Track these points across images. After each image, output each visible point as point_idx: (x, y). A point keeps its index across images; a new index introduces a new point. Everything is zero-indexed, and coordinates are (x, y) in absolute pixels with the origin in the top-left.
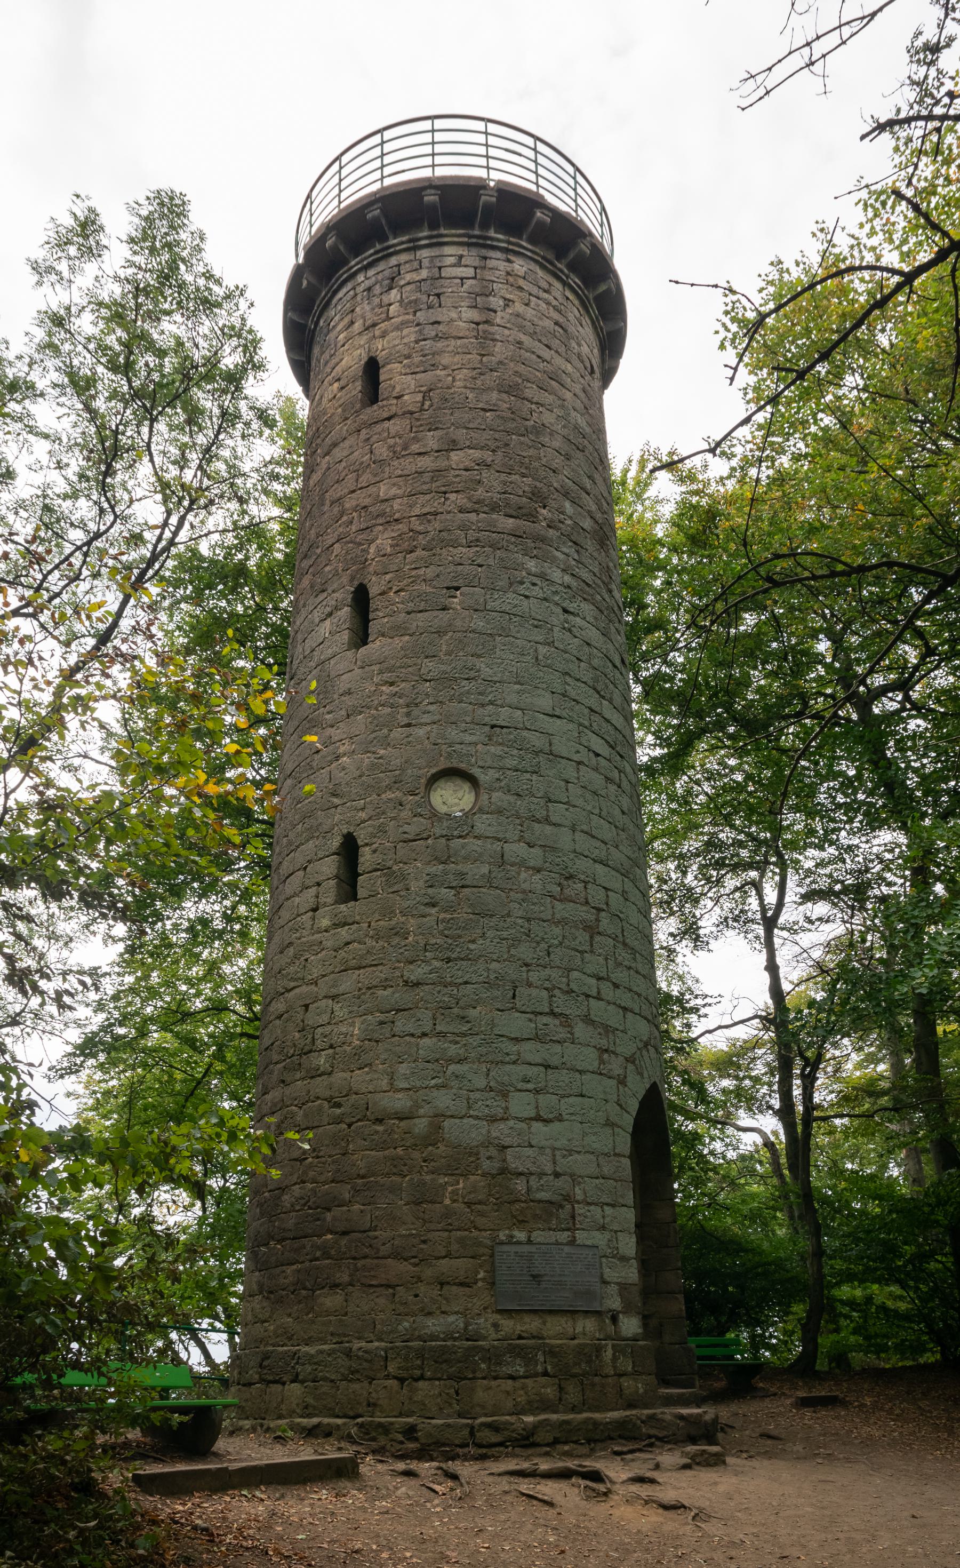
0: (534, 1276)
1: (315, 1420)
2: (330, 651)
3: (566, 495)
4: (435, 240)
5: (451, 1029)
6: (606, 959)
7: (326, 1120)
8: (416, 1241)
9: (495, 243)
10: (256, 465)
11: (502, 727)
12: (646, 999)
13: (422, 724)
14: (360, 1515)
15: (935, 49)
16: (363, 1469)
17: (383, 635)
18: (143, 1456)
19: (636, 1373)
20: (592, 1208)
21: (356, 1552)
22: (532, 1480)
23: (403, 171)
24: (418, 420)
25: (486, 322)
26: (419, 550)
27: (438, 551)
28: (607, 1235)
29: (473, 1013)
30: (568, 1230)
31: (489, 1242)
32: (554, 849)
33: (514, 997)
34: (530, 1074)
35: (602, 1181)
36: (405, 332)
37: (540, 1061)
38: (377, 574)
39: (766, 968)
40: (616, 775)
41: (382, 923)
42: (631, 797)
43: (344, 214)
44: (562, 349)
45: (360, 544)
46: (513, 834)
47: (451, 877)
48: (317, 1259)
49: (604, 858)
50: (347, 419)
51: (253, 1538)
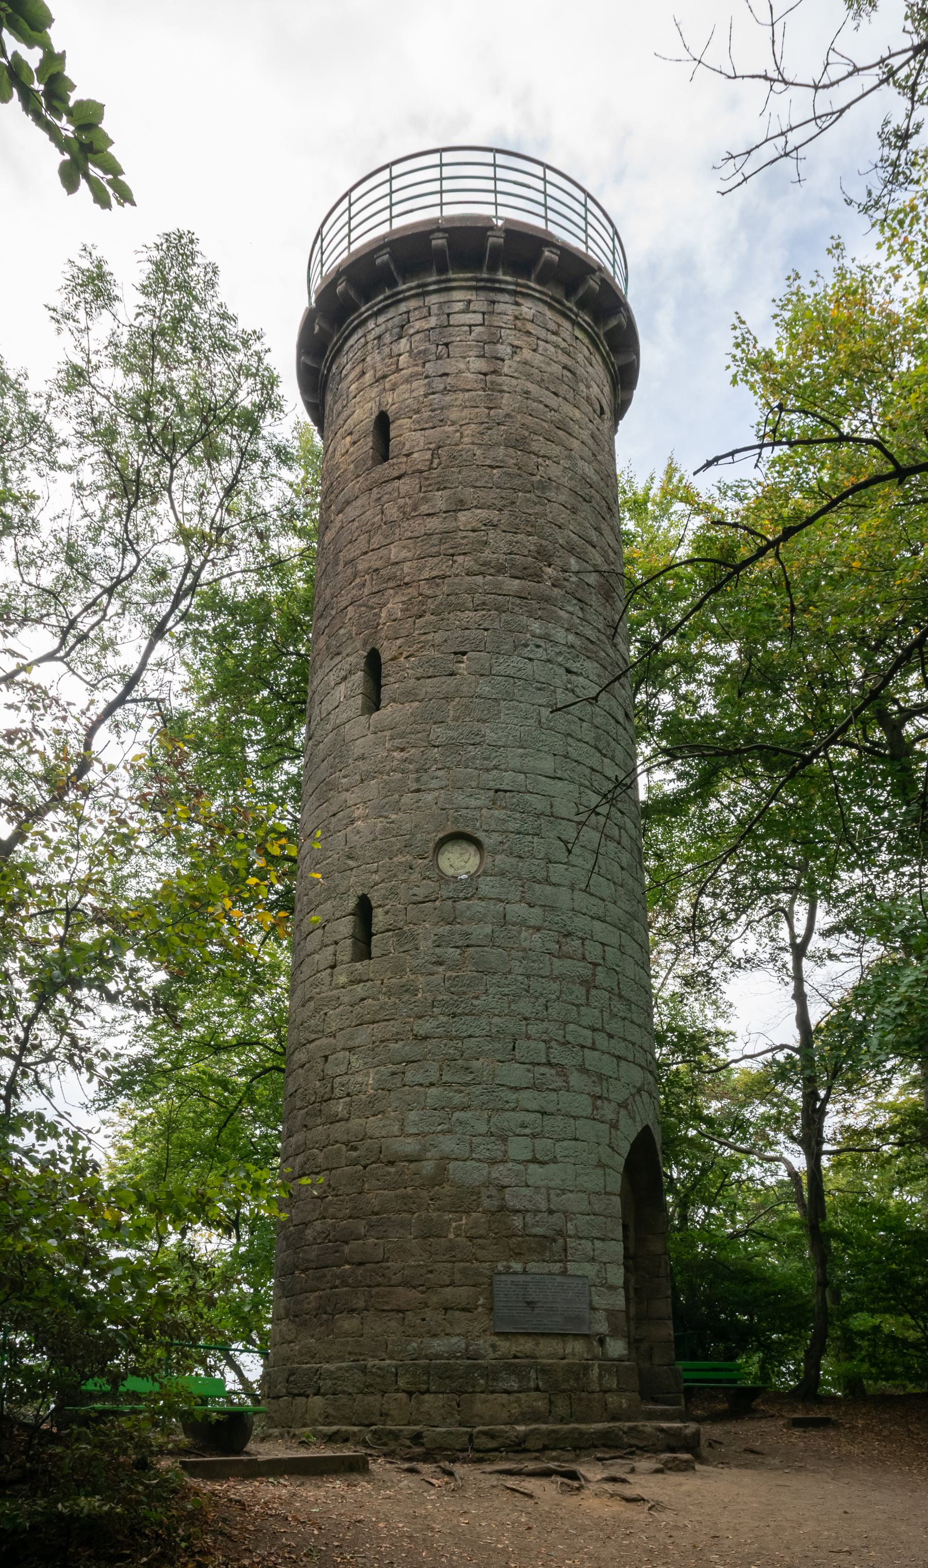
0: (529, 1303)
1: (335, 1428)
2: (345, 715)
3: (571, 550)
4: (443, 285)
5: (456, 1079)
6: (602, 1011)
7: (344, 1162)
8: (423, 1271)
9: (503, 286)
10: (275, 502)
11: (506, 791)
12: (641, 1047)
13: (430, 790)
14: (365, 1499)
15: (904, 137)
16: (372, 1466)
17: (394, 701)
18: (187, 1452)
19: (620, 1390)
20: (583, 1241)
21: (359, 1522)
22: (518, 1478)
23: (411, 211)
24: (427, 479)
25: (494, 372)
26: (428, 614)
27: (446, 615)
28: (597, 1266)
29: (476, 1064)
30: (560, 1261)
31: (488, 1273)
32: (553, 908)
33: (514, 1049)
34: (527, 1120)
35: (593, 1217)
36: (415, 384)
37: (537, 1108)
38: (387, 638)
39: (794, 997)
40: (615, 832)
41: (393, 980)
42: (631, 853)
43: (354, 258)
44: (570, 396)
45: (372, 608)
46: (515, 895)
47: (457, 936)
48: (336, 1287)
49: (601, 914)
50: (359, 476)
51: (276, 1509)
